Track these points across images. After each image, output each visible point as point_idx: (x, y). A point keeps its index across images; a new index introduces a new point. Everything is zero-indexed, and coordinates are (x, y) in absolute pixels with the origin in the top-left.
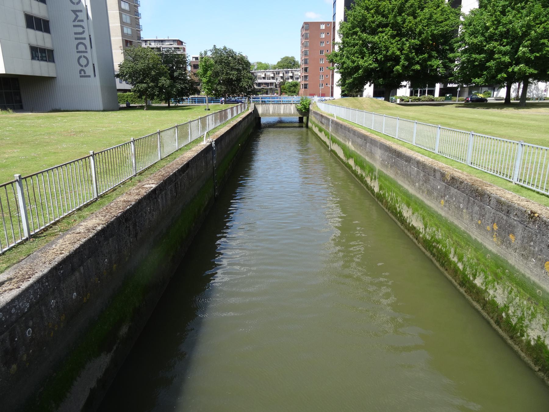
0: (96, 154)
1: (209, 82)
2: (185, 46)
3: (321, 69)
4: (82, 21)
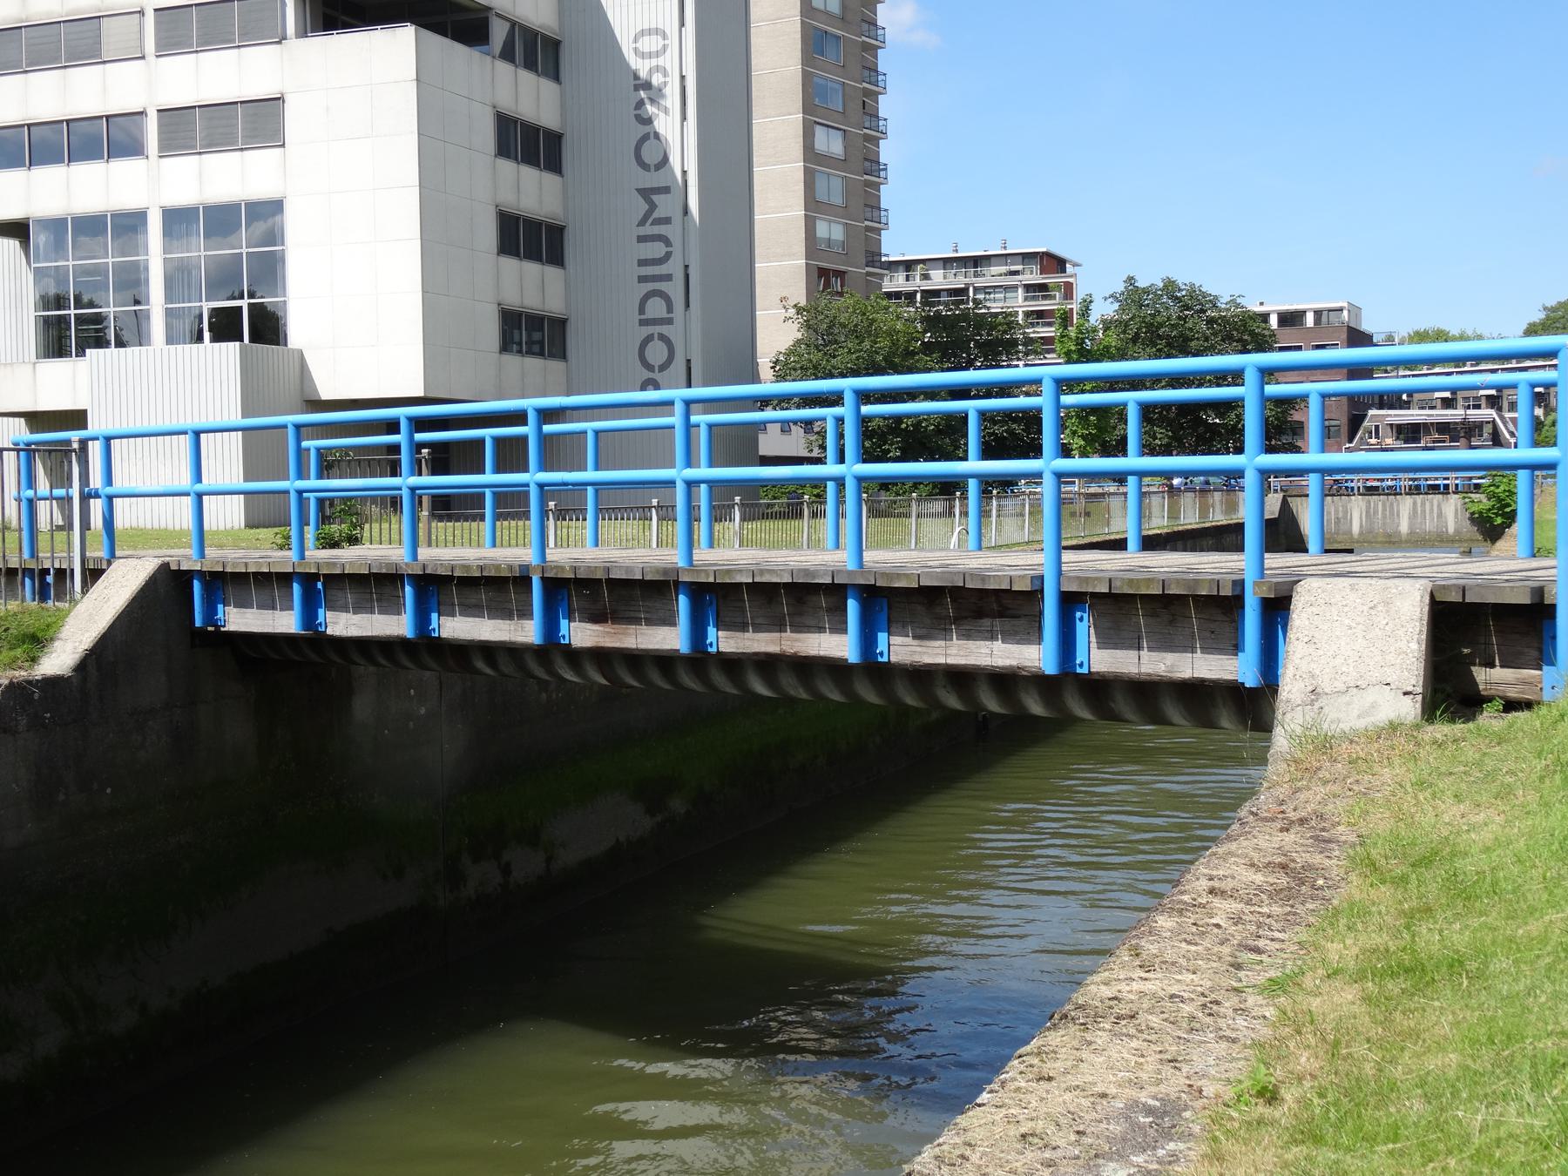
0: (662, 507)
4: (667, 221)
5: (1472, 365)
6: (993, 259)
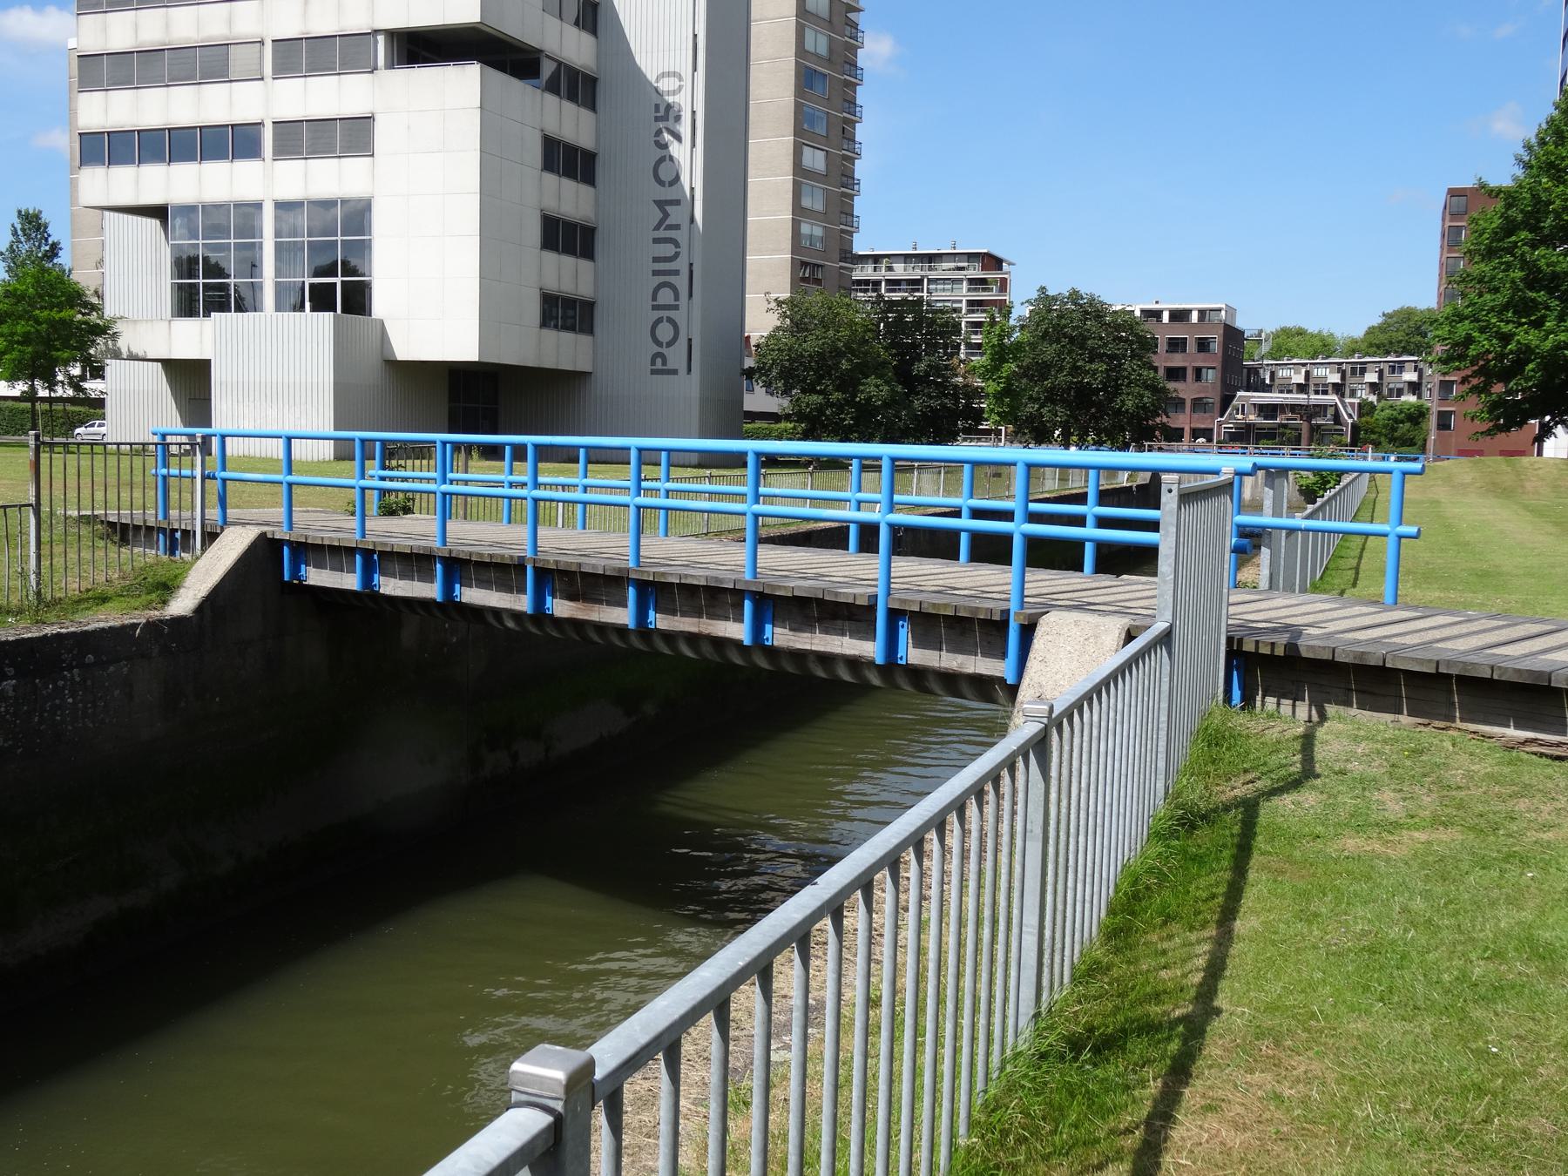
1: (1007, 391)
2: (1009, 273)
4: (677, 227)
5: (1323, 359)
6: (944, 257)
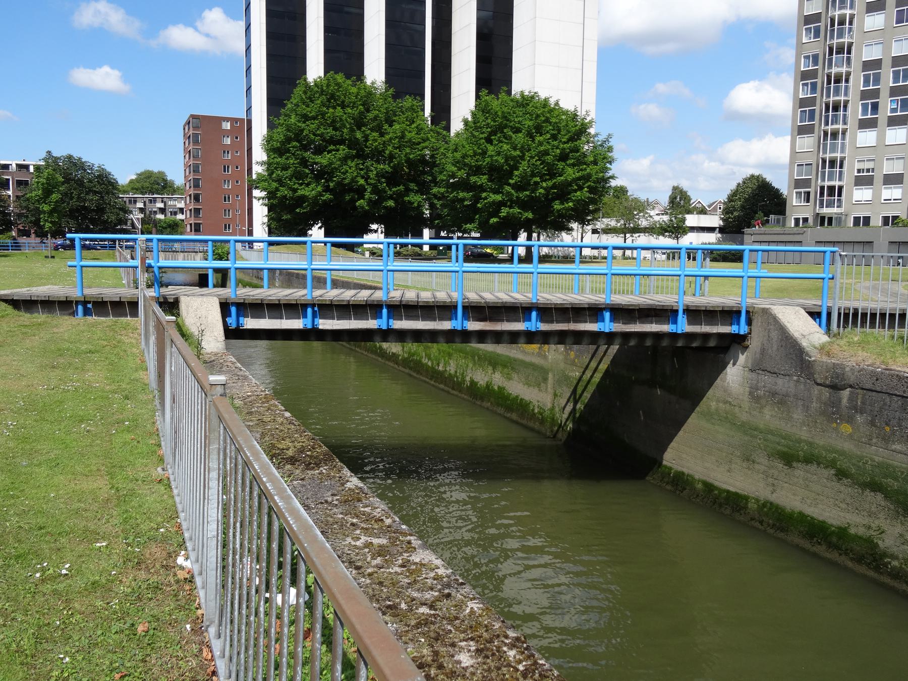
3: (225, 198)
